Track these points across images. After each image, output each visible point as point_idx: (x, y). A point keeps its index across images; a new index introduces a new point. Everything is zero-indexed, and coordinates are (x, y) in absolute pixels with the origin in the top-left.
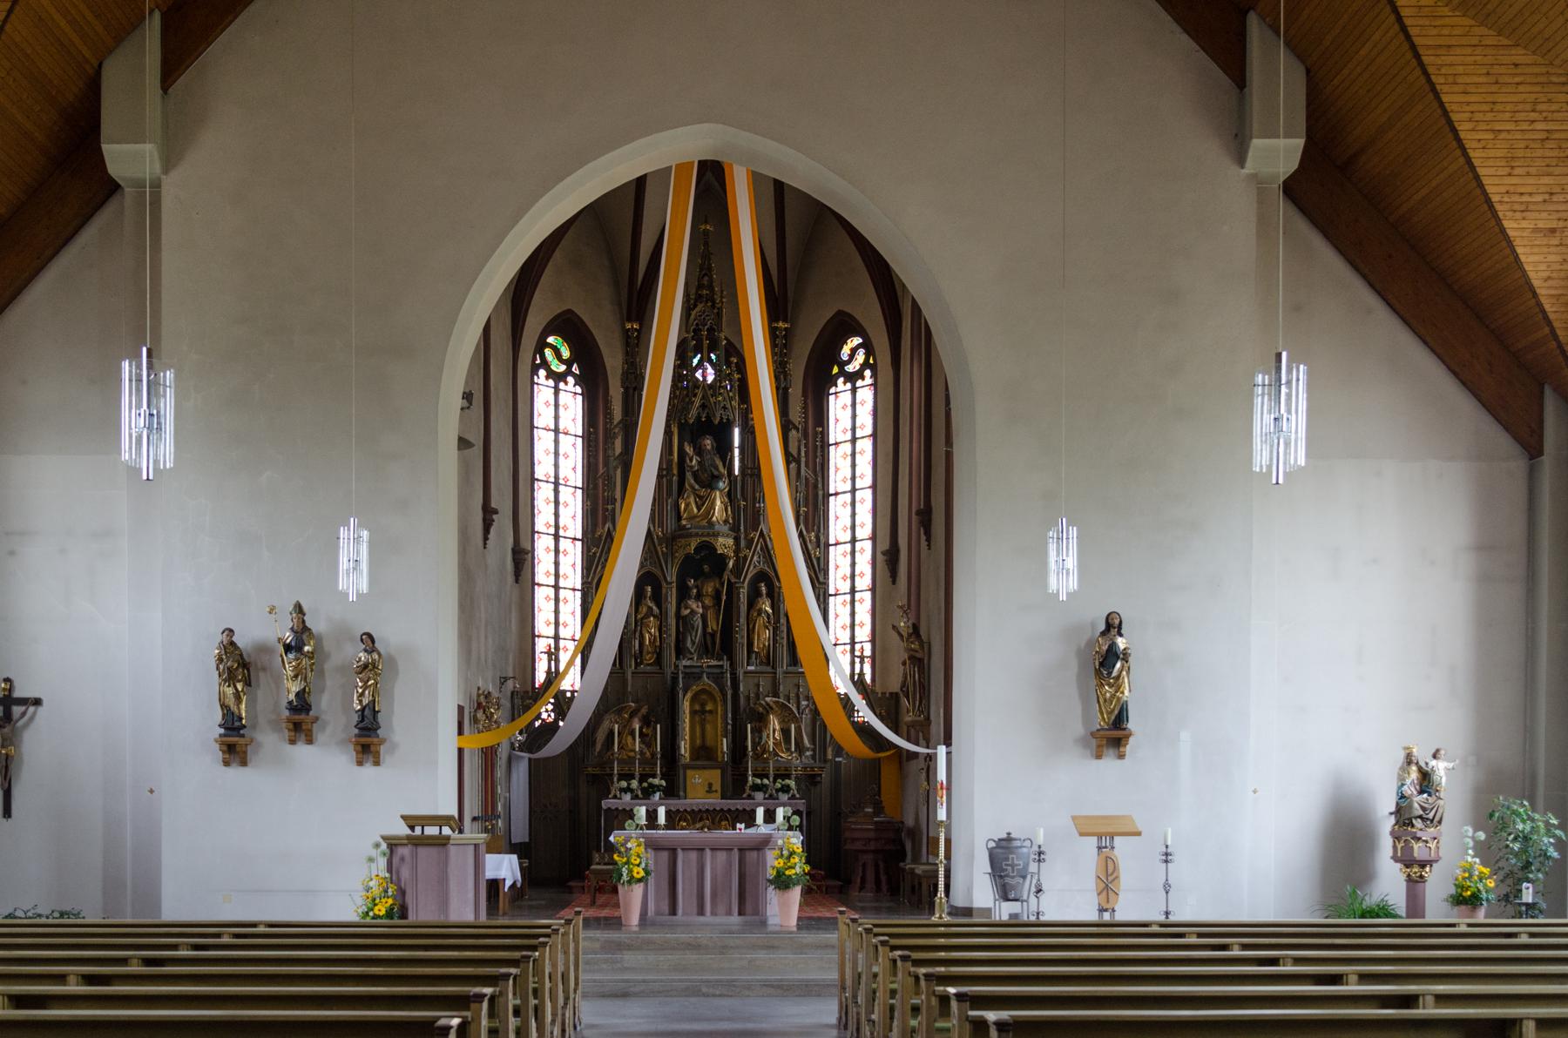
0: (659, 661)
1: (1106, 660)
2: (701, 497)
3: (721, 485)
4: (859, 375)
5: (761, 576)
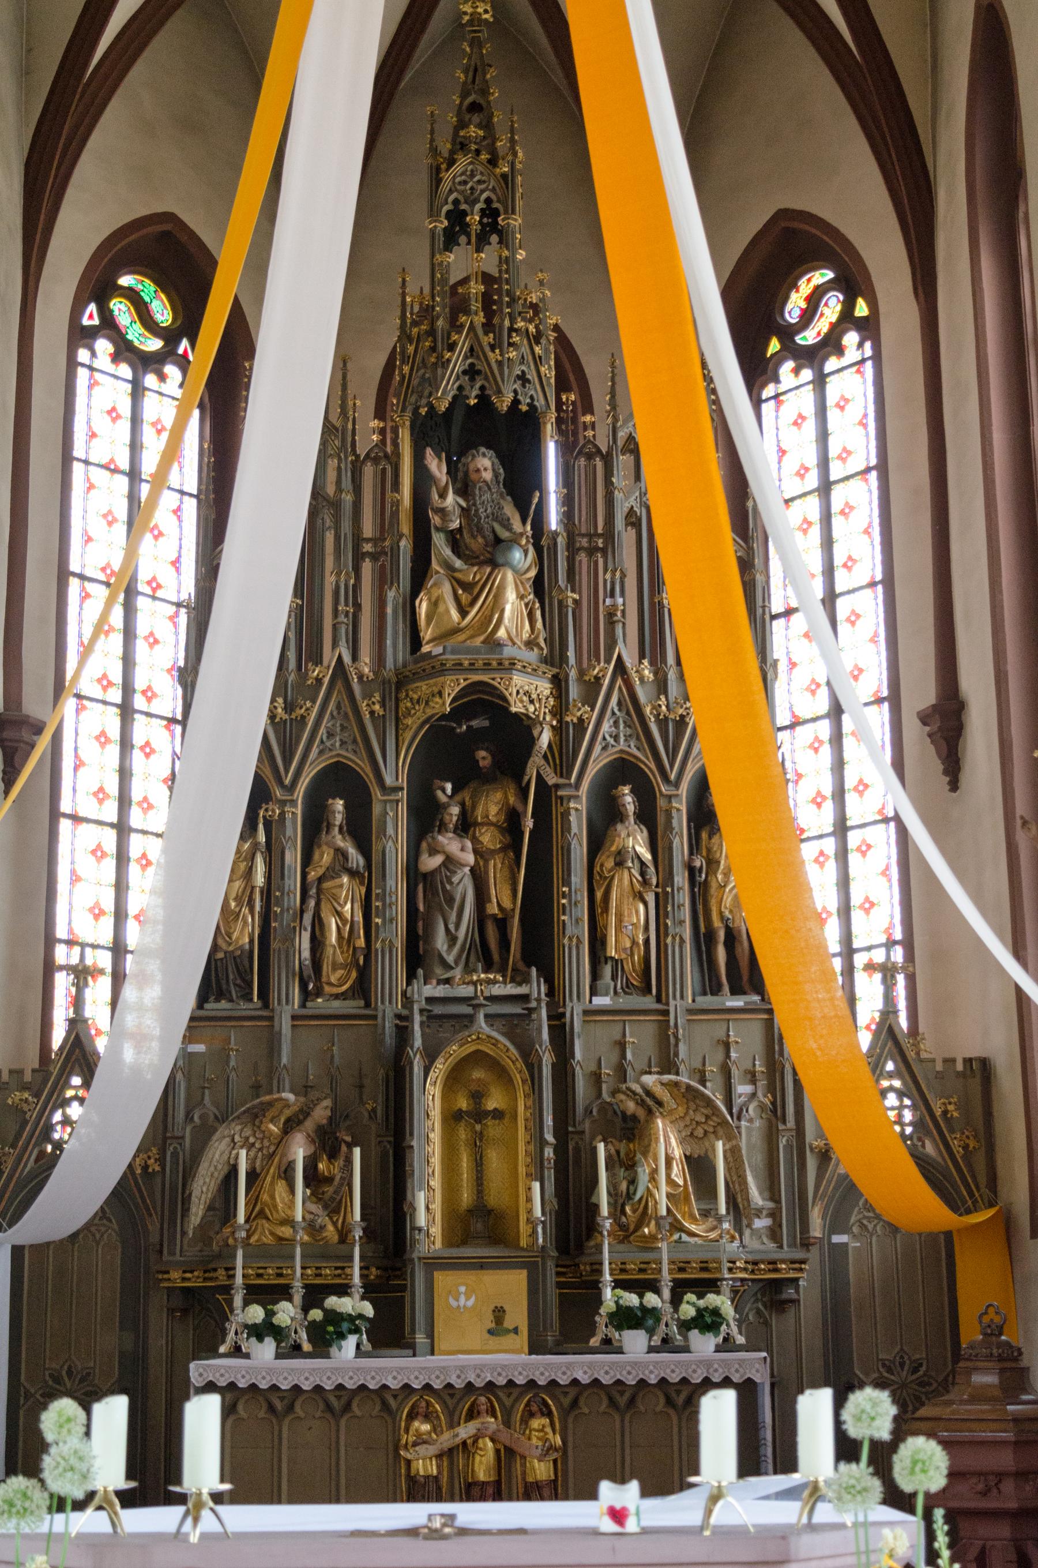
0: (362, 988)
2: (467, 587)
3: (517, 555)
4: (832, 343)
5: (622, 770)
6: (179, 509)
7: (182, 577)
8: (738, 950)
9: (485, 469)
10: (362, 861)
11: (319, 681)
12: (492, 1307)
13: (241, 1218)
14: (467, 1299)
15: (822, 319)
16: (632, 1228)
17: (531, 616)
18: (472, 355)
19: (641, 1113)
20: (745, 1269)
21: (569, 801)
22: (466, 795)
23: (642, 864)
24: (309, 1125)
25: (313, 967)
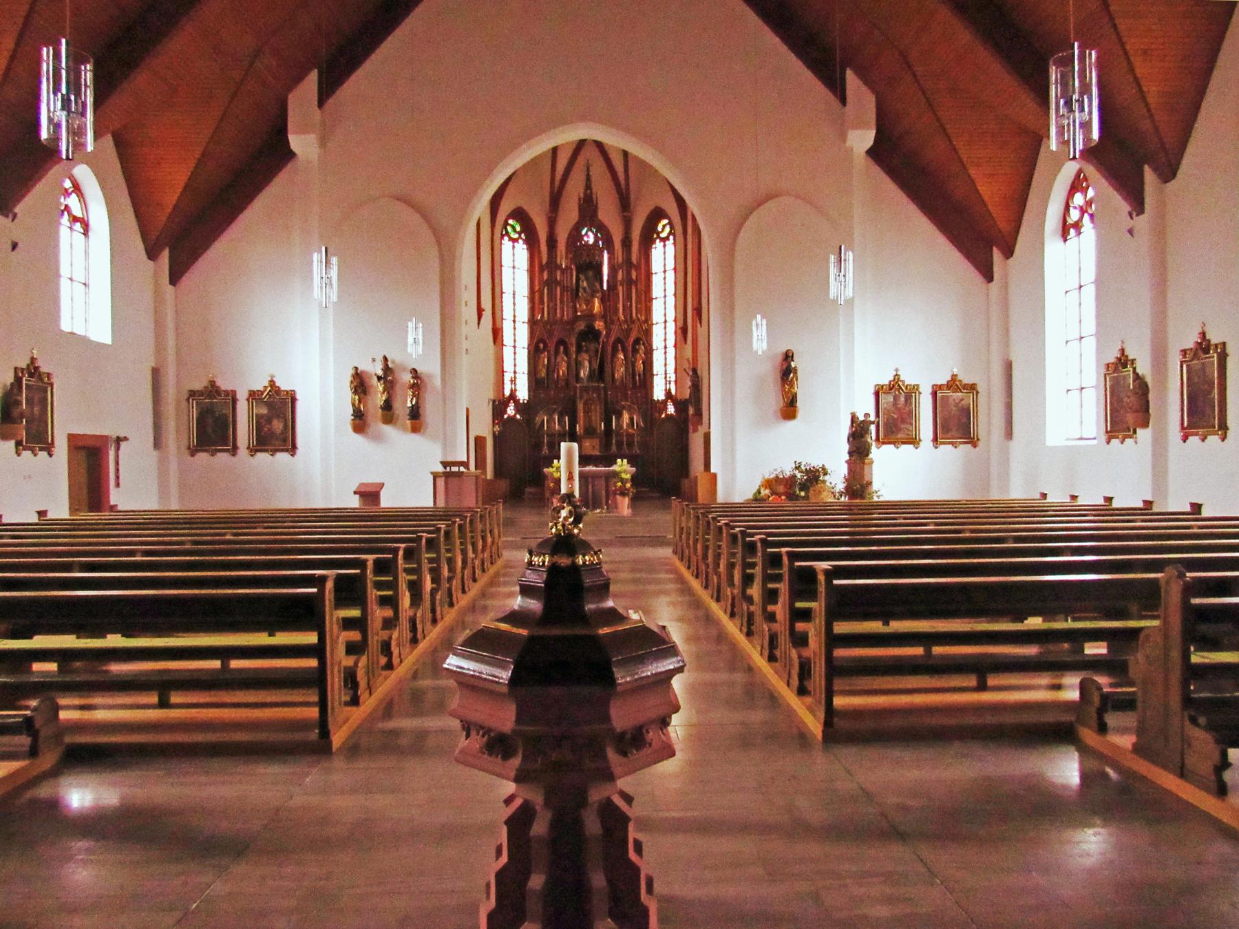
1: (786, 371)
4: (667, 238)
5: (618, 340)
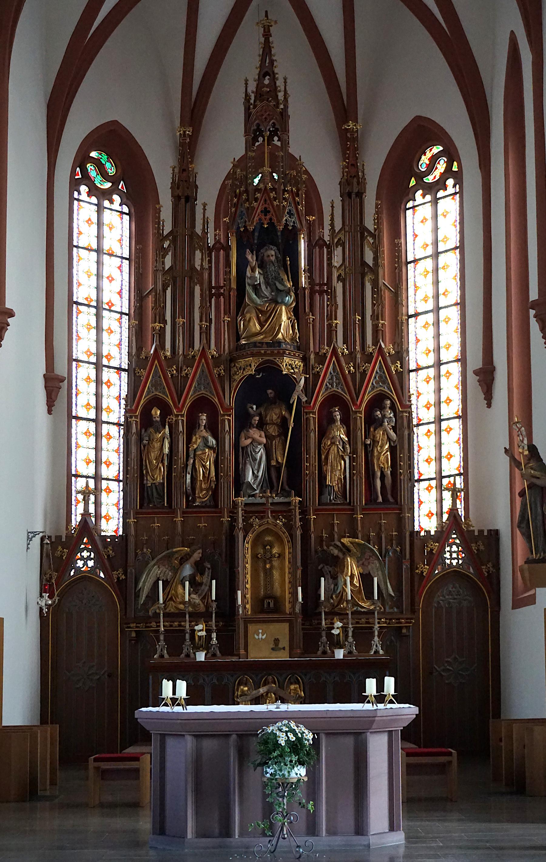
4: (441, 184)
5: (334, 400)
6: (121, 266)
7: (123, 300)
8: (386, 481)
9: (272, 256)
10: (214, 442)
11: (194, 356)
12: (273, 639)
13: (161, 601)
14: (263, 635)
15: (437, 171)
16: (336, 604)
17: (293, 327)
18: (265, 204)
19: (341, 555)
20: (385, 623)
21: (310, 414)
22: (262, 410)
23: (343, 442)
24: (192, 560)
25: (192, 490)
